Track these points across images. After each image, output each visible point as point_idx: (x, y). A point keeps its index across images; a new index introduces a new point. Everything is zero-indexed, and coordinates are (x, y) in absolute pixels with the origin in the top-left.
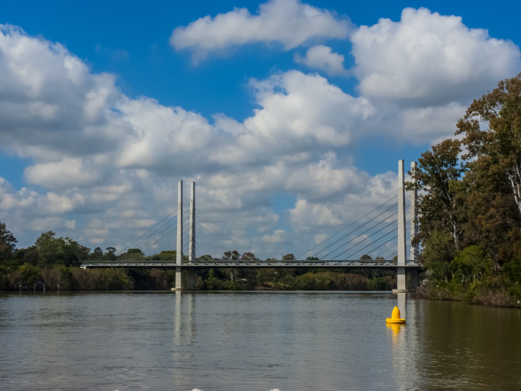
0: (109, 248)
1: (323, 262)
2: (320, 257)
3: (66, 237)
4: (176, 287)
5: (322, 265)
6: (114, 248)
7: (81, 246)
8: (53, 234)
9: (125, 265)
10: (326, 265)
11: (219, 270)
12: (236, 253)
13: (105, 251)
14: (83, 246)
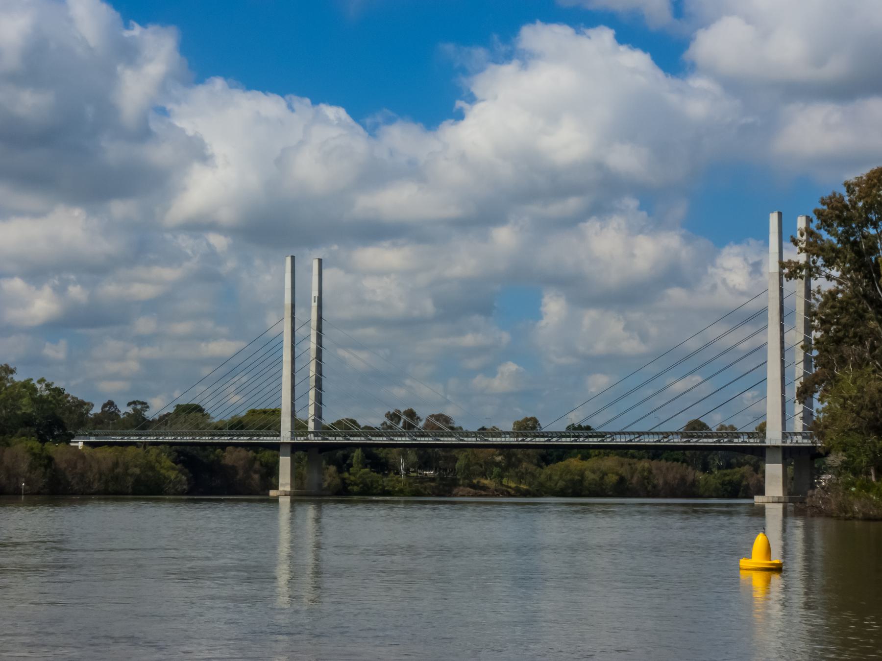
0: (134, 403)
1: (602, 435)
2: (596, 423)
3: (39, 378)
4: (281, 488)
5: (210, 440)
6: (145, 403)
7: (73, 398)
8: (12, 372)
9: (169, 439)
10: (608, 441)
11: (375, 451)
12: (411, 414)
13: (124, 410)
14: (77, 398)
